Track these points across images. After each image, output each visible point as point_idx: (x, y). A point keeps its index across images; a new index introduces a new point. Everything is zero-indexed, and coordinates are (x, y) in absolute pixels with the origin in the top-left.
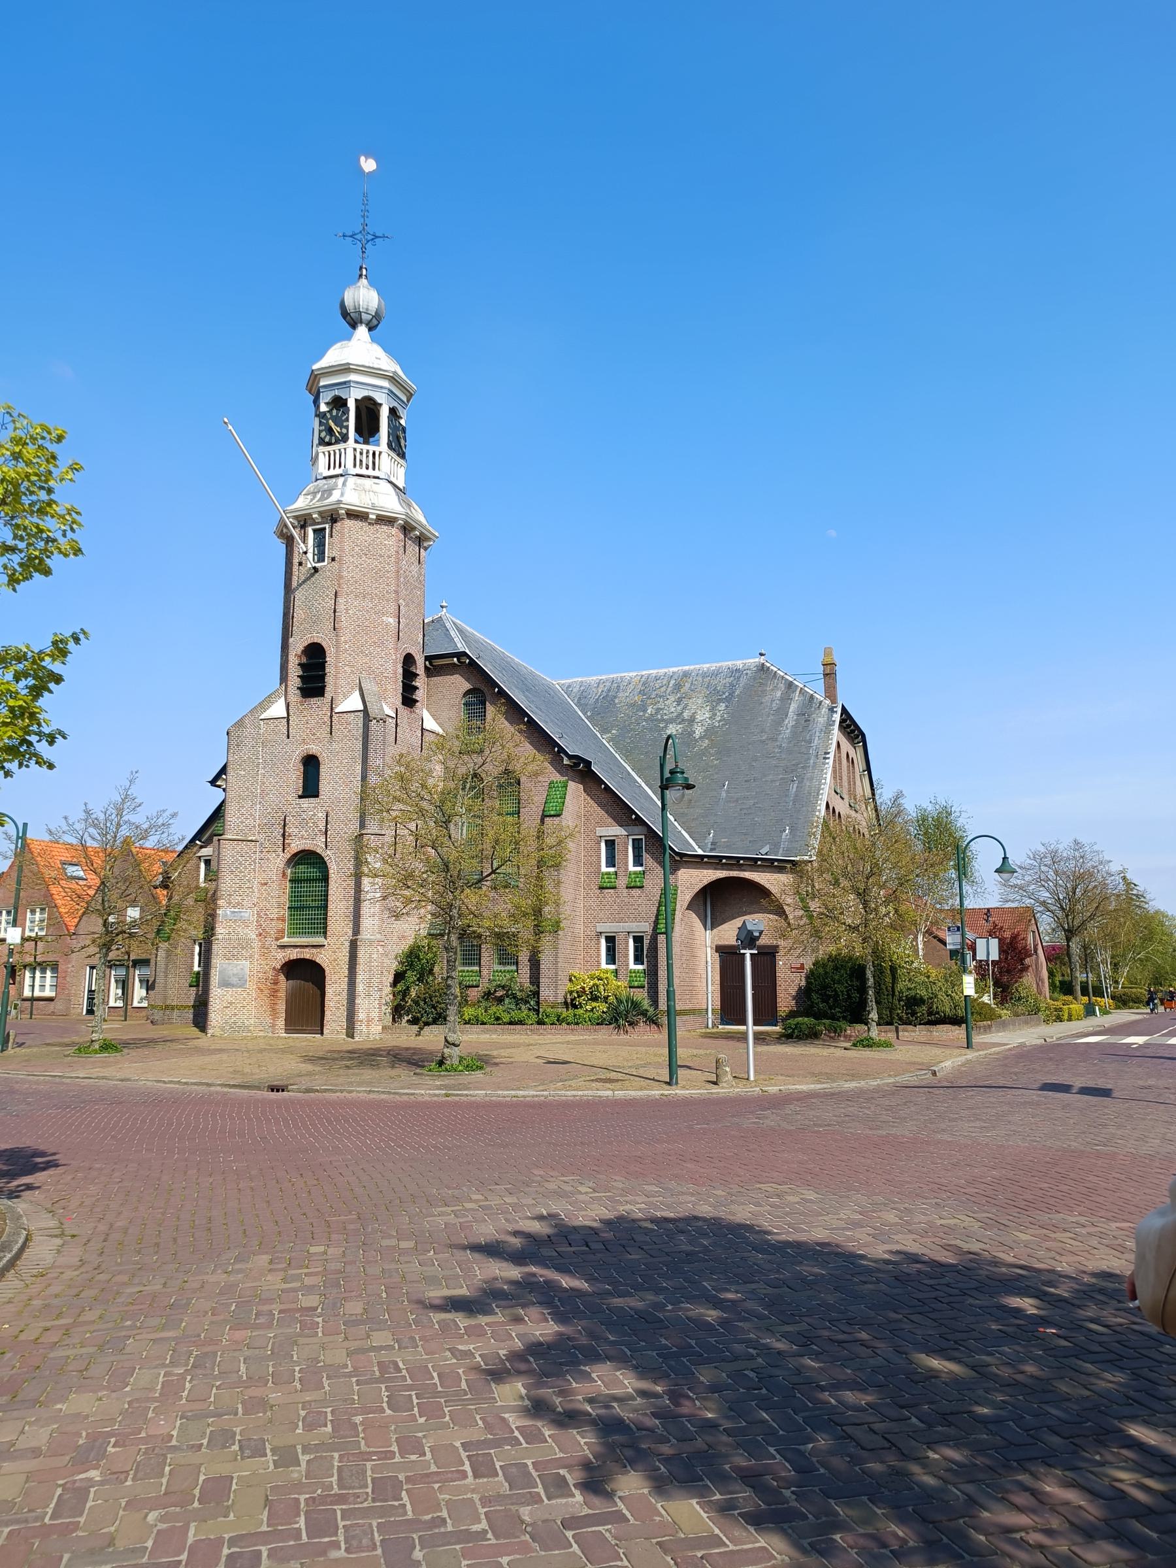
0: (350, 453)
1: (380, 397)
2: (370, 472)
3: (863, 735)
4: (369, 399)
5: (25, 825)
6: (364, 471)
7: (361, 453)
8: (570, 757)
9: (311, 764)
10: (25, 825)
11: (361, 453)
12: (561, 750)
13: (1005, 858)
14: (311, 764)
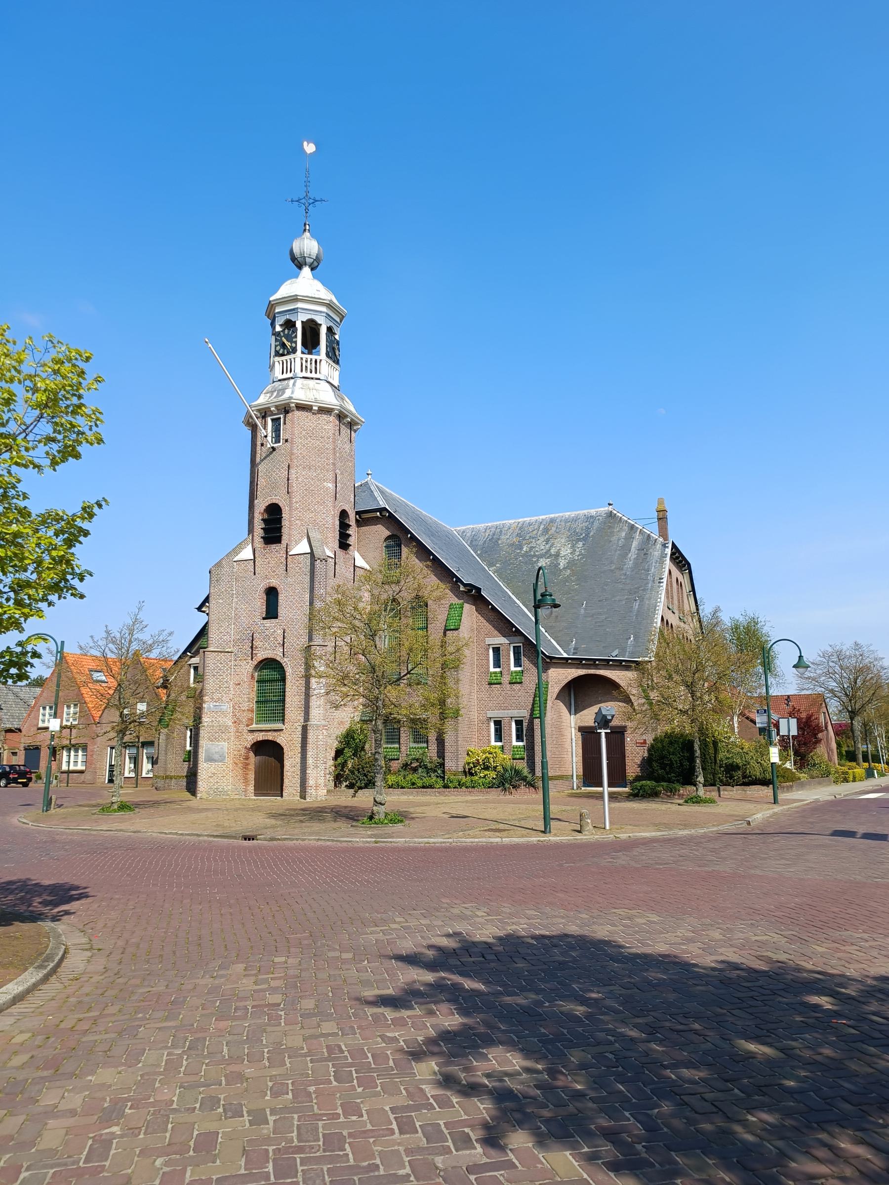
0: (298, 361)
1: (320, 319)
2: (313, 375)
3: (689, 565)
4: (312, 321)
5: (63, 643)
6: (308, 375)
7: (306, 361)
8: (465, 585)
9: (272, 593)
10: (63, 643)
11: (306, 361)
12: (458, 580)
13: (800, 657)
14: (272, 593)
